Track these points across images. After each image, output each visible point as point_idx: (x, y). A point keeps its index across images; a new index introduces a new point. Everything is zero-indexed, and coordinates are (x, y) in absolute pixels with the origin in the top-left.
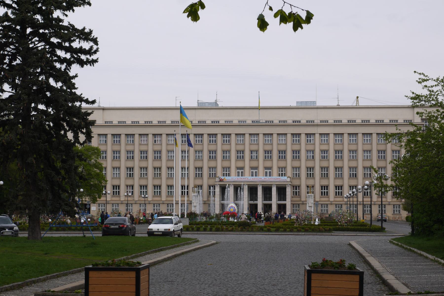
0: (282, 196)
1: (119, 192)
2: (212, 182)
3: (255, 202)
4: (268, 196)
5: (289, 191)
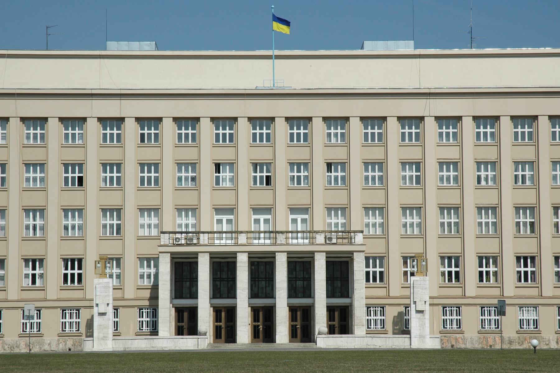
0: (338, 284)
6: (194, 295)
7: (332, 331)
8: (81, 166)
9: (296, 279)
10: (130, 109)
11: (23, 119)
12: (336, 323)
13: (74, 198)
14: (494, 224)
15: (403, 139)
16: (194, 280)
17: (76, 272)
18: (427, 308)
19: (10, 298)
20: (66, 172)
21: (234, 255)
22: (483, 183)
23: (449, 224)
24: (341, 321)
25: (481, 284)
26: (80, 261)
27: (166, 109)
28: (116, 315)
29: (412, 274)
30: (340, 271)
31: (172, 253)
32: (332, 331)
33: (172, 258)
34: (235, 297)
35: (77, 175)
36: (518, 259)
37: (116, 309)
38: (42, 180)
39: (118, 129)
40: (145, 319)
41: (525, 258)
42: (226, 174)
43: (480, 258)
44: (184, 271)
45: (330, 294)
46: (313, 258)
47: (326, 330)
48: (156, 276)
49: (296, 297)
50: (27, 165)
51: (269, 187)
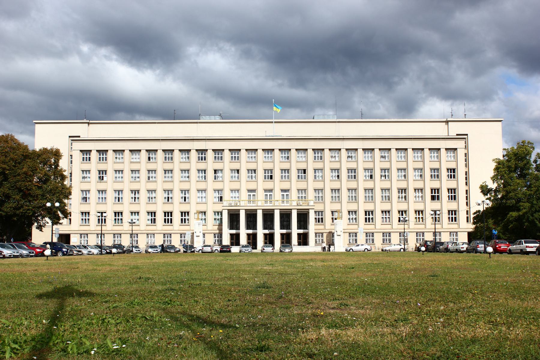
2: (219, 208)
4: (285, 223)
5: (312, 216)
7: (299, 244)
8: (271, 170)
9: (284, 221)
11: (180, 150)
12: (234, 241)
13: (269, 185)
14: (422, 197)
17: (454, 216)
18: (342, 234)
19: (158, 229)
21: (256, 210)
22: (317, 178)
23: (335, 197)
24: (303, 240)
25: (366, 223)
28: (204, 237)
29: (336, 219)
30: (303, 218)
31: (228, 210)
32: (299, 244)
33: (246, 212)
34: (256, 229)
35: (270, 174)
36: (416, 211)
37: (204, 234)
38: (172, 177)
39: (122, 155)
40: (217, 239)
41: (419, 211)
42: (219, 174)
44: (234, 218)
46: (291, 212)
47: (297, 244)
48: (221, 219)
50: (116, 171)
51: (271, 180)
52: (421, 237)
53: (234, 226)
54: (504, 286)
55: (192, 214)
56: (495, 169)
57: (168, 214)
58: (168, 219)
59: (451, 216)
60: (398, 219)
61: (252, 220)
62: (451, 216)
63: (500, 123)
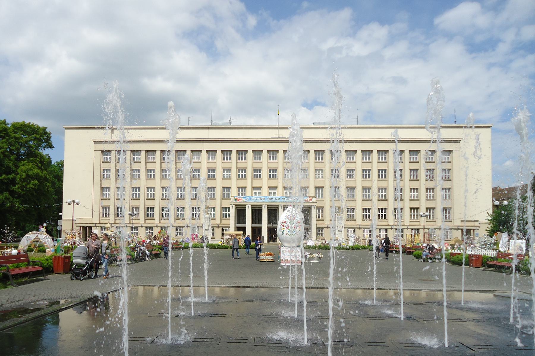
1: (153, 214)
3: (274, 226)
5: (314, 213)
6: (244, 223)
10: (219, 147)
15: (316, 159)
16: (244, 216)
20: (255, 172)
21: (261, 206)
26: (153, 208)
27: (234, 147)
30: (273, 213)
34: (261, 224)
43: (363, 209)
44: (240, 213)
45: (269, 223)
49: (240, 224)
52: (384, 233)
53: (241, 221)
54: (521, 283)
55: (201, 209)
56: (51, 137)
57: (151, 209)
58: (382, 215)
59: (365, 213)
60: (155, 215)
61: (257, 215)
62: (365, 213)
63: (489, 129)
